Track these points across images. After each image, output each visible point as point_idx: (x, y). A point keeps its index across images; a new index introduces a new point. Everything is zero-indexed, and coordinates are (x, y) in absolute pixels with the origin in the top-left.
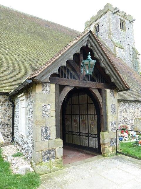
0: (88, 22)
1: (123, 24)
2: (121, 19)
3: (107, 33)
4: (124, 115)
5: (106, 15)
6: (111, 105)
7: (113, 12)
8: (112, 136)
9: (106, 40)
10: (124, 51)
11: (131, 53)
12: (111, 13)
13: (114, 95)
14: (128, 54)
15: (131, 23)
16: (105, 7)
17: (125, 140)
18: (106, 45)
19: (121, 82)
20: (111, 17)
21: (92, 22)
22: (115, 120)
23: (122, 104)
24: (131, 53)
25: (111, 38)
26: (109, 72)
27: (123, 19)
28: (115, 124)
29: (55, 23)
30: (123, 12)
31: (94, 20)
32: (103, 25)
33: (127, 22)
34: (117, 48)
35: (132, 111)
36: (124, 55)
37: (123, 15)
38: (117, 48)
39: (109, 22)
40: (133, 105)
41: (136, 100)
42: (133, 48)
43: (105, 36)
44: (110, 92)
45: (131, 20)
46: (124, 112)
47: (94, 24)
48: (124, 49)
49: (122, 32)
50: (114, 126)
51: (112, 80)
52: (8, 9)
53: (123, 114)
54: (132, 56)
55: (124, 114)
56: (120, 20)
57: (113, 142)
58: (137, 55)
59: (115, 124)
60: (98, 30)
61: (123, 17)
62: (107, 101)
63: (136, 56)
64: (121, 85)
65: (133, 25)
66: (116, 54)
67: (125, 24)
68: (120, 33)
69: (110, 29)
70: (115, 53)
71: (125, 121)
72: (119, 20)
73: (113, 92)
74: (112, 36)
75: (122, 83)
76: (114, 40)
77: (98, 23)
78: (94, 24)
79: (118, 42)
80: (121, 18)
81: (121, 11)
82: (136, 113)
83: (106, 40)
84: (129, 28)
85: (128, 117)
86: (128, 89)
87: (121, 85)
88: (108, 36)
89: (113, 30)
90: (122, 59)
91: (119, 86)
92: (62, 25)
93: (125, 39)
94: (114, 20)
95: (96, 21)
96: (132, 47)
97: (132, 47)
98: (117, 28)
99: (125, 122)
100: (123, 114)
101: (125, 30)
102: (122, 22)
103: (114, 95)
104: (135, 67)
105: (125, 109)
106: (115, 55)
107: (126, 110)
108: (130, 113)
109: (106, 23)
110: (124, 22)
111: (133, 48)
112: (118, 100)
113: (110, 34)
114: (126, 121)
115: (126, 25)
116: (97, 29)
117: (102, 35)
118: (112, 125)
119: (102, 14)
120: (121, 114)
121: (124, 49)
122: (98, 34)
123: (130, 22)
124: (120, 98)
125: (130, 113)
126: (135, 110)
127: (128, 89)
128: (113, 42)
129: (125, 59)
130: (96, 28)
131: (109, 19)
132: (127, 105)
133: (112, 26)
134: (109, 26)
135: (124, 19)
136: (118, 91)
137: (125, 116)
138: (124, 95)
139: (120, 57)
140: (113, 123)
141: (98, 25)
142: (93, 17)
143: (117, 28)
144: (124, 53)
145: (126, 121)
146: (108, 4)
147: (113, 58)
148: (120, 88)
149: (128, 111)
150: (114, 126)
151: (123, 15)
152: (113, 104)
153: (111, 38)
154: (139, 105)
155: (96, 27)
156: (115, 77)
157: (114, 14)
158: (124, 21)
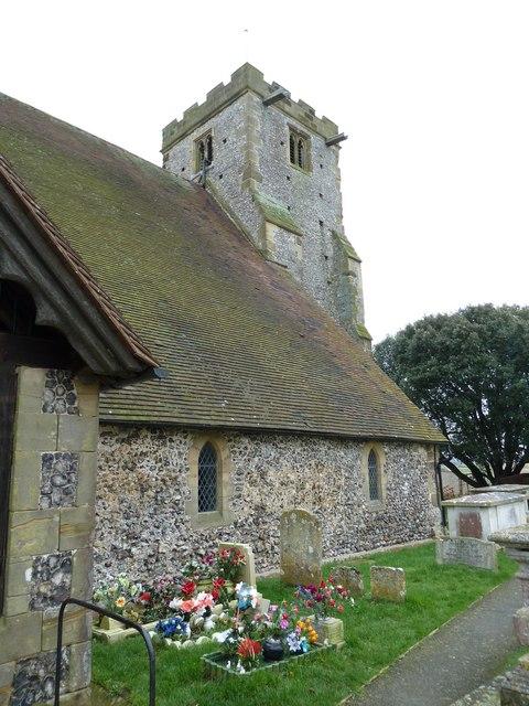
0: (174, 123)
1: (300, 147)
2: (292, 129)
3: (240, 172)
4: (254, 495)
5: (239, 105)
6: (47, 459)
7: (262, 97)
8: (30, 642)
9: (234, 195)
10: (299, 243)
11: (330, 253)
12: (257, 99)
13: (72, 399)
14: (316, 257)
15: (333, 147)
16: (236, 76)
17: (198, 629)
18: (232, 214)
19: (103, 329)
20: (256, 115)
21: (187, 126)
22: (66, 546)
23: (246, 448)
24: (330, 253)
25: (250, 190)
26: (25, 270)
27: (300, 127)
28: (66, 565)
29: (18, 102)
30: (301, 103)
31: (197, 120)
32: (225, 141)
33: (316, 142)
34: (272, 230)
35: (292, 477)
36: (300, 258)
37: (303, 115)
38: (272, 230)
39: (247, 130)
40: (298, 450)
41: (308, 429)
42: (335, 235)
43: (232, 180)
44: (49, 385)
45: (331, 137)
46: (252, 483)
47: (196, 135)
48: (301, 235)
49: (296, 172)
50: (58, 579)
51: (45, 315)
52: (503, 331)
53: (246, 488)
54: (330, 264)
55: (255, 491)
56: (290, 129)
57: (35, 677)
58: (350, 261)
59: (63, 565)
60: (210, 157)
61: (301, 120)
62: (18, 435)
63: (346, 265)
64: (107, 346)
65: (337, 157)
66: (266, 252)
67: (309, 146)
68: (288, 178)
69: (249, 155)
70: (264, 244)
71: (256, 523)
72: (287, 128)
73: (68, 385)
74: (256, 184)
75: (110, 338)
76: (263, 198)
77: (210, 131)
78: (196, 135)
79: (280, 206)
80: (294, 123)
81: (295, 98)
82: (308, 486)
83: (234, 195)
84: (324, 164)
85: (272, 505)
86: (145, 371)
87: (107, 346)
88: (241, 182)
89: (261, 162)
90: (292, 269)
91: (89, 348)
92: (50, 113)
93: (308, 202)
94: (269, 126)
95: (203, 122)
96: (333, 232)
97: (333, 232)
98: (276, 156)
99: (257, 524)
100: (246, 488)
101: (309, 169)
102: (297, 140)
103: (72, 399)
104: (340, 306)
105: (258, 468)
106: (262, 254)
107: (263, 475)
108: (282, 484)
109: (238, 133)
110: (308, 140)
111: (335, 235)
112: (103, 423)
113: (248, 173)
114: (264, 523)
115: (313, 153)
116: (206, 154)
117: (221, 177)
118: (43, 572)
119: (222, 99)
120: (238, 489)
121: (301, 235)
122: (206, 172)
123: (328, 145)
124: (110, 414)
125: (282, 484)
126: (307, 470)
127: (145, 371)
128: (259, 204)
129: (301, 272)
130: (202, 150)
131: (249, 120)
132: (268, 451)
133: (256, 148)
134: (248, 147)
135: (306, 131)
136: (109, 381)
137: (257, 500)
138: (132, 400)
139: (284, 262)
140: (47, 564)
141: (210, 139)
142: (195, 109)
143: (276, 156)
144: (298, 248)
145: (264, 523)
146: (247, 66)
147: (253, 265)
148: (101, 362)
149: (272, 475)
150: (58, 579)
151: (303, 115)
152: (63, 450)
153: (250, 190)
154: (323, 449)
155: (202, 146)
156: (56, 295)
157: (266, 104)
158: (306, 137)
